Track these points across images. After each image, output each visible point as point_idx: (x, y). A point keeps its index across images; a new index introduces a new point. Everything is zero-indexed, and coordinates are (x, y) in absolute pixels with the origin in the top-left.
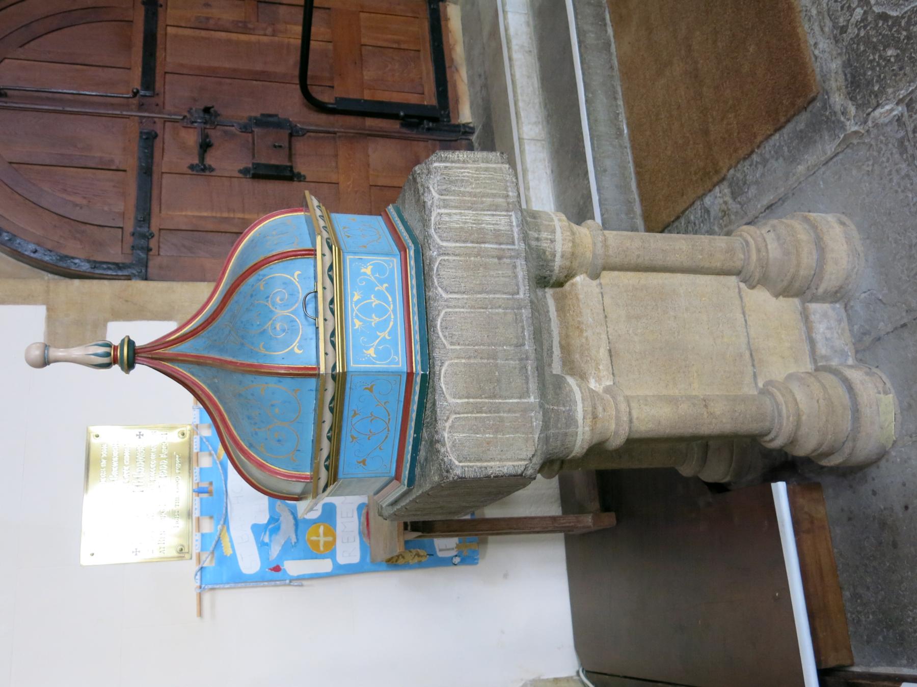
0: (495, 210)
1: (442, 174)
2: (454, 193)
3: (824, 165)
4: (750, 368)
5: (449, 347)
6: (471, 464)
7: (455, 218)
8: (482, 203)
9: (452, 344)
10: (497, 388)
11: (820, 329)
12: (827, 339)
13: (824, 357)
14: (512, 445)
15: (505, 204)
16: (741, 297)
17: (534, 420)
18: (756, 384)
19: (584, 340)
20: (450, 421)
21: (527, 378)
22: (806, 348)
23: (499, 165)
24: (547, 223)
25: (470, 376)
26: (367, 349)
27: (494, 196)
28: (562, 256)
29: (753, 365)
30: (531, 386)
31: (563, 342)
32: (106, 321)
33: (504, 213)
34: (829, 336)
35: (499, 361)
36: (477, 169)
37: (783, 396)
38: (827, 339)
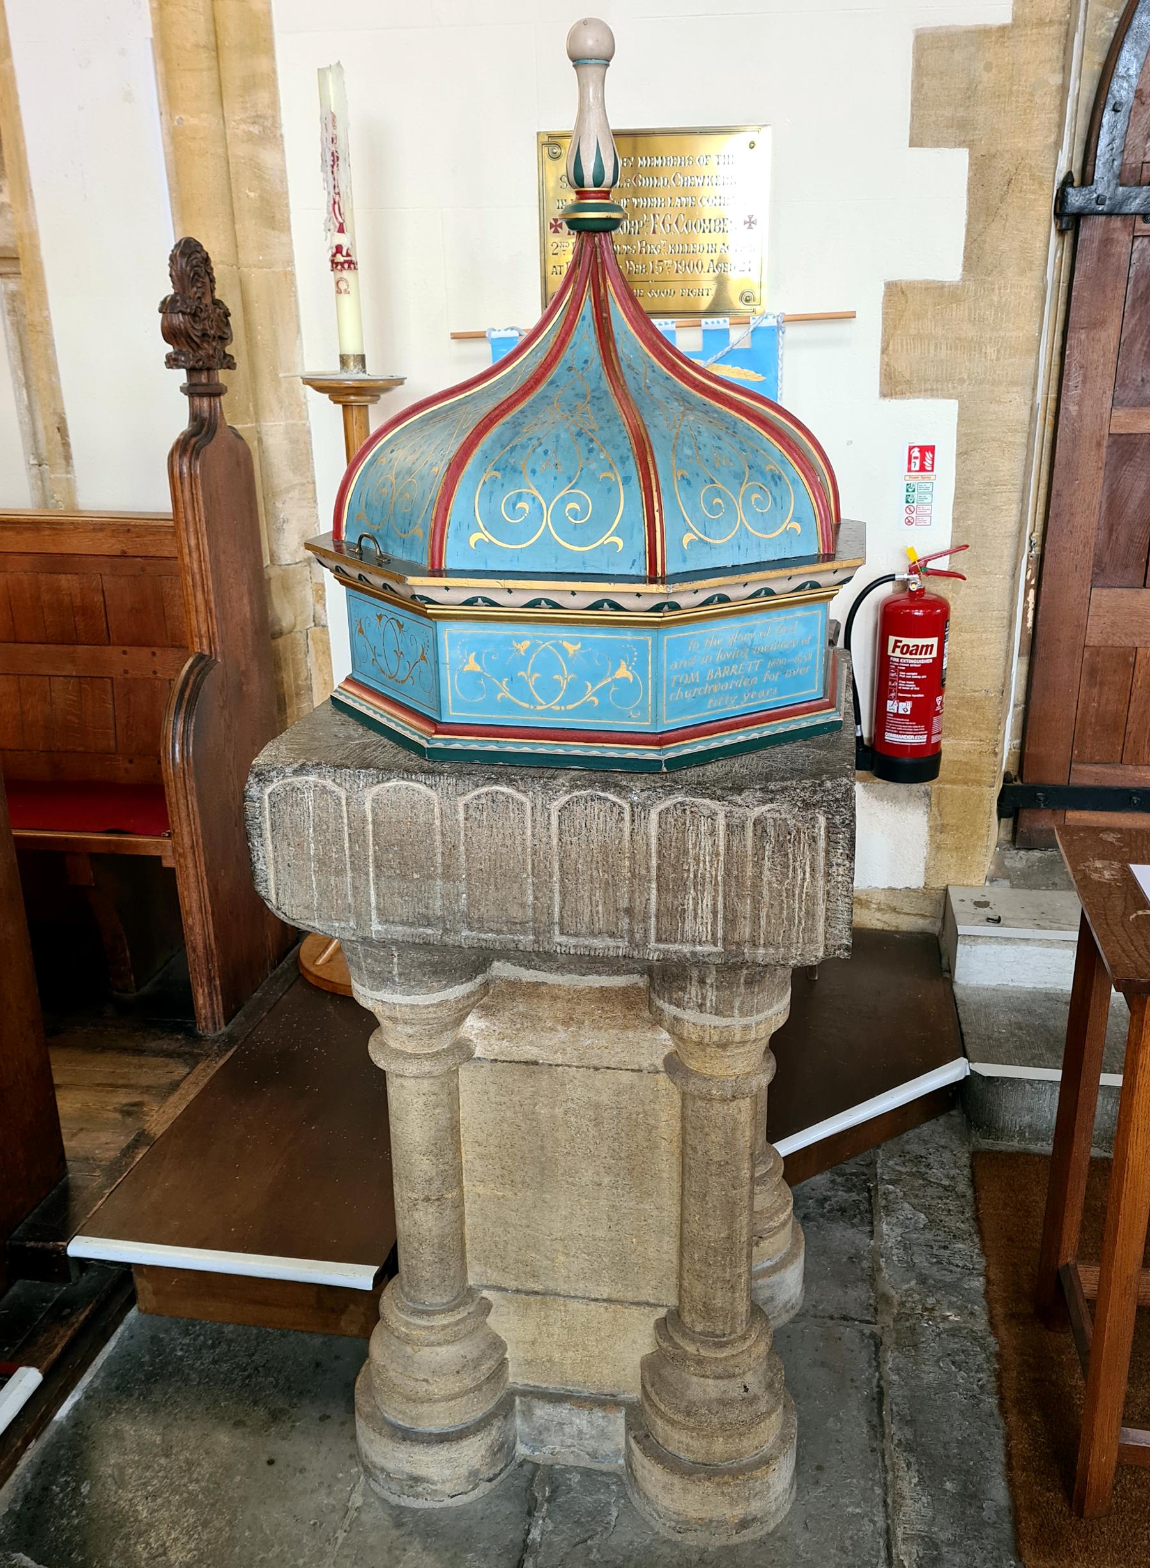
0: (725, 918)
1: (798, 831)
2: (759, 850)
3: (888, 1530)
4: (514, 1284)
5: (462, 801)
6: (267, 813)
7: (706, 843)
8: (740, 897)
9: (467, 806)
10: (391, 873)
11: (580, 1420)
12: (561, 1424)
13: (528, 1413)
14: (300, 882)
15: (737, 938)
16: (638, 1304)
17: (343, 924)
18: (488, 1287)
19: (549, 1024)
20: (335, 788)
21: (412, 924)
22: (552, 1386)
23: (821, 939)
24: (737, 1004)
25: (409, 830)
26: (478, 659)
27: (756, 919)
28: (676, 1018)
29: (518, 1291)
30: (400, 928)
31: (544, 989)
32: (971, 145)
33: (720, 934)
34: (567, 1429)
35: (439, 882)
36: (812, 897)
37: (444, 1327)
38: (561, 1424)
